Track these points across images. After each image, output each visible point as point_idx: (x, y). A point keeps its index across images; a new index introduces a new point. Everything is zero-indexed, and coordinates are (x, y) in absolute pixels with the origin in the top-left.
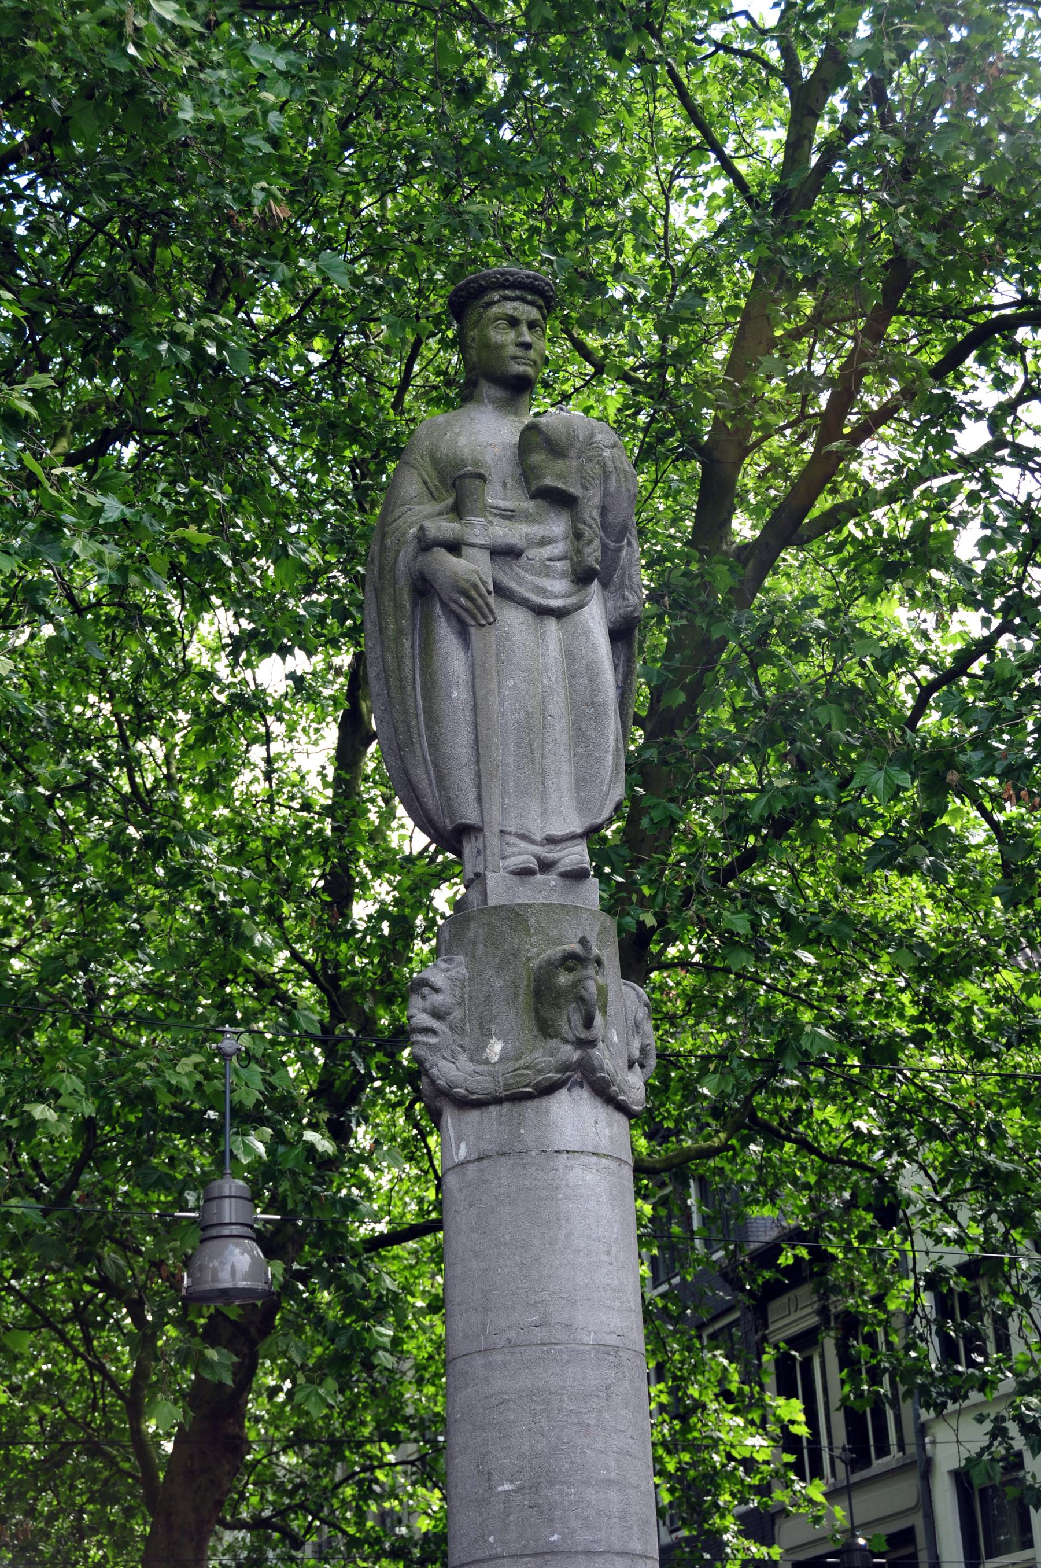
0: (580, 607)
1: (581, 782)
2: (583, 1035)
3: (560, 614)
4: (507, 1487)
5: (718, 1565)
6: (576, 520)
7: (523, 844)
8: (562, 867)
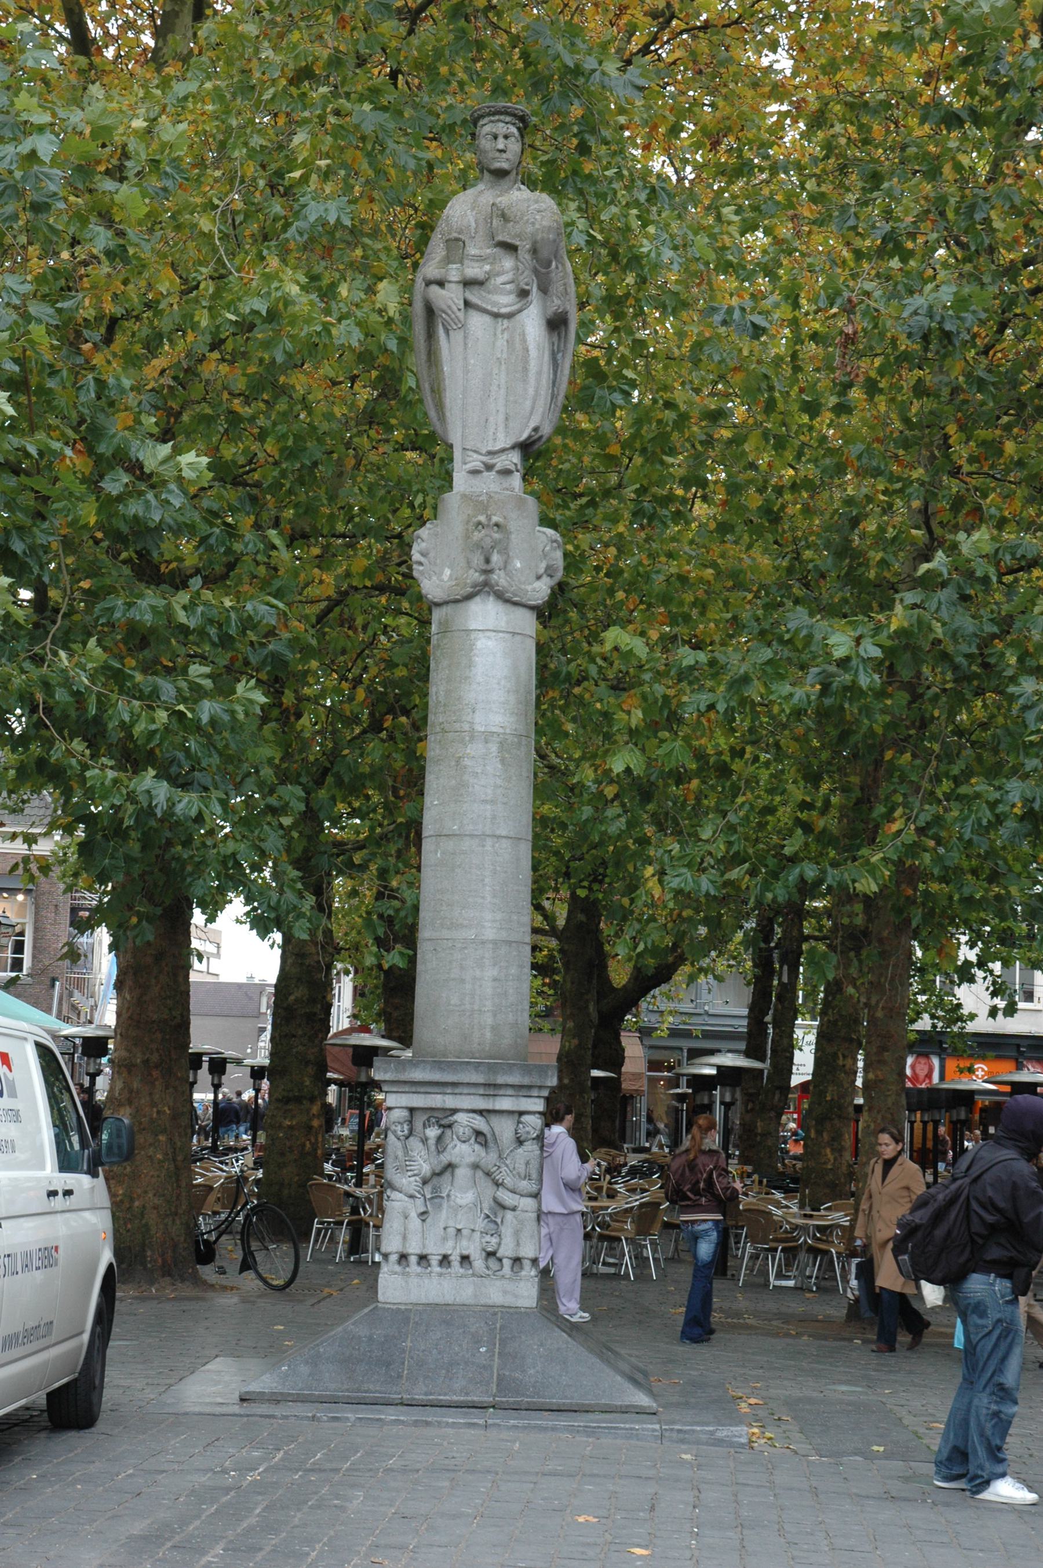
0: (520, 311)
3: (510, 316)
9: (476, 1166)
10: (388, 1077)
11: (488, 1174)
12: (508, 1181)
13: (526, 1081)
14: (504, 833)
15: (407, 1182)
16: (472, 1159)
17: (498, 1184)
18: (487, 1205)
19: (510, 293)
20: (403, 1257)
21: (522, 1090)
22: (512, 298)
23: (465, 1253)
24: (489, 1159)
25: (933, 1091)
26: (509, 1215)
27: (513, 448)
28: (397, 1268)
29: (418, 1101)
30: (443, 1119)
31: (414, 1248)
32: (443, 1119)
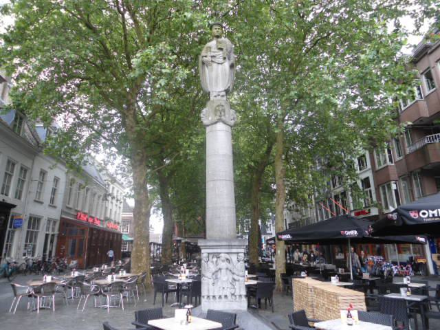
3: (221, 64)
9: (227, 269)
11: (230, 271)
13: (240, 244)
15: (209, 274)
16: (225, 267)
18: (230, 280)
20: (208, 297)
21: (239, 246)
24: (230, 266)
25: (363, 243)
26: (237, 283)
28: (226, 300)
32: (217, 255)
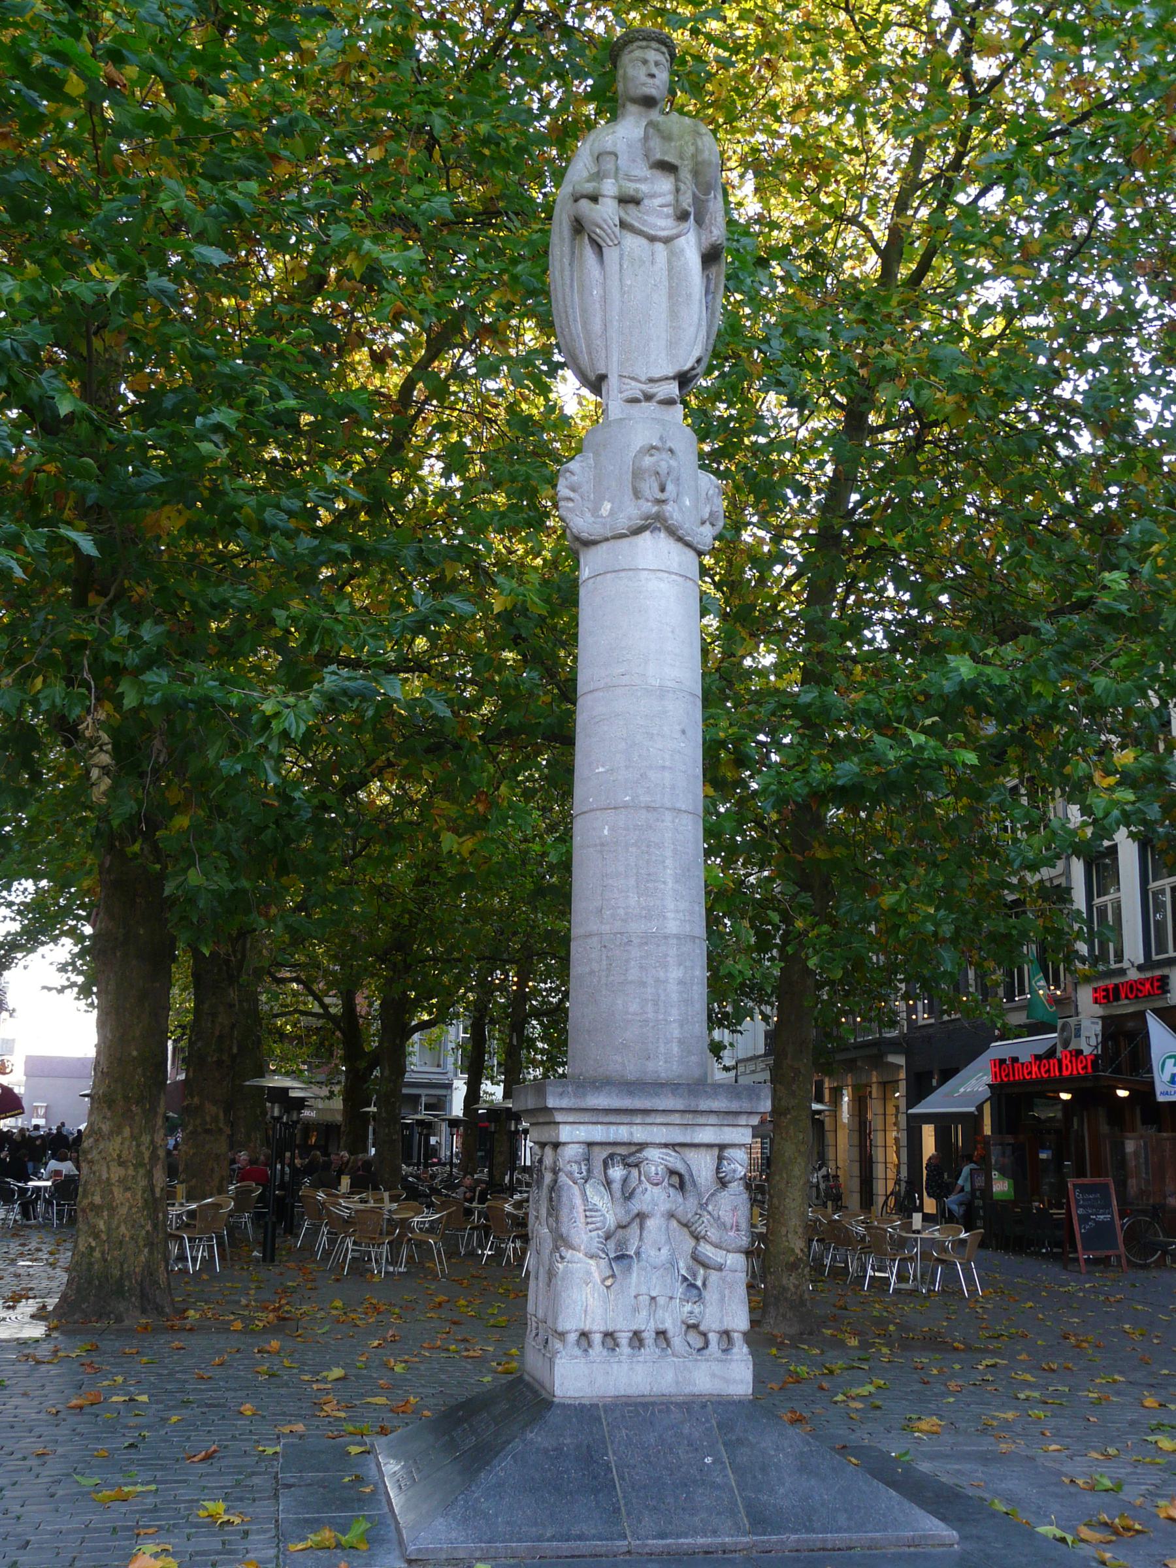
0: (678, 236)
1: (672, 344)
2: (660, 496)
3: (667, 241)
4: (601, 770)
5: (1171, 617)
6: (677, 180)
7: (633, 383)
8: (658, 398)
10: (565, 1103)
12: (713, 1234)
13: (734, 1106)
14: (683, 807)
15: (583, 1235)
17: (697, 1238)
19: (667, 216)
21: (729, 1116)
22: (670, 222)
23: (661, 1327)
24: (687, 1206)
26: (714, 1276)
27: (674, 378)
29: (598, 1133)
30: (630, 1155)
31: (596, 1325)
32: (630, 1155)
